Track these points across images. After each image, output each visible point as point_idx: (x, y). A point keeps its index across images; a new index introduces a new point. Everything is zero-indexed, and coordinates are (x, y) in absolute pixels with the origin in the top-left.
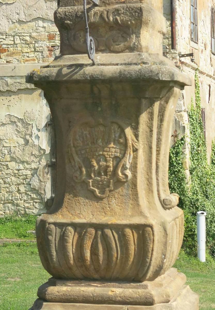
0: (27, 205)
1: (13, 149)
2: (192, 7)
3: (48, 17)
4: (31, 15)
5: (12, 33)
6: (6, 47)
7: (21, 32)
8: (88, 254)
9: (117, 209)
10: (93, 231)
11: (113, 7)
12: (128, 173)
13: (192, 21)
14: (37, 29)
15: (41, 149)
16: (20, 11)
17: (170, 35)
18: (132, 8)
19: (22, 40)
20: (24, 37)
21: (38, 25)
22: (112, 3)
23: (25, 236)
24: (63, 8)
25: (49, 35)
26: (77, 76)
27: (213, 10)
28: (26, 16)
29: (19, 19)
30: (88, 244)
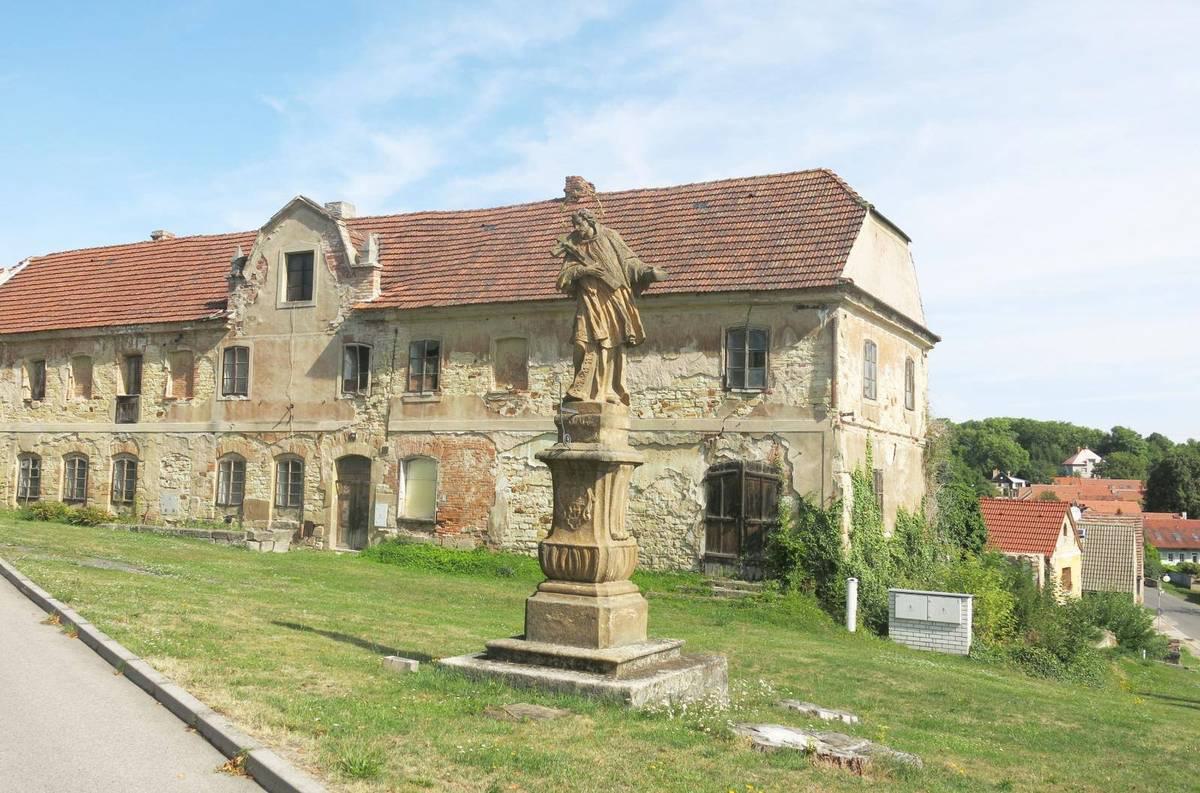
0: (681, 560)
1: (670, 504)
8: (554, 561)
9: (582, 538)
10: (566, 549)
12: (589, 515)
15: (697, 504)
23: (673, 591)
26: (559, 457)
30: (564, 557)
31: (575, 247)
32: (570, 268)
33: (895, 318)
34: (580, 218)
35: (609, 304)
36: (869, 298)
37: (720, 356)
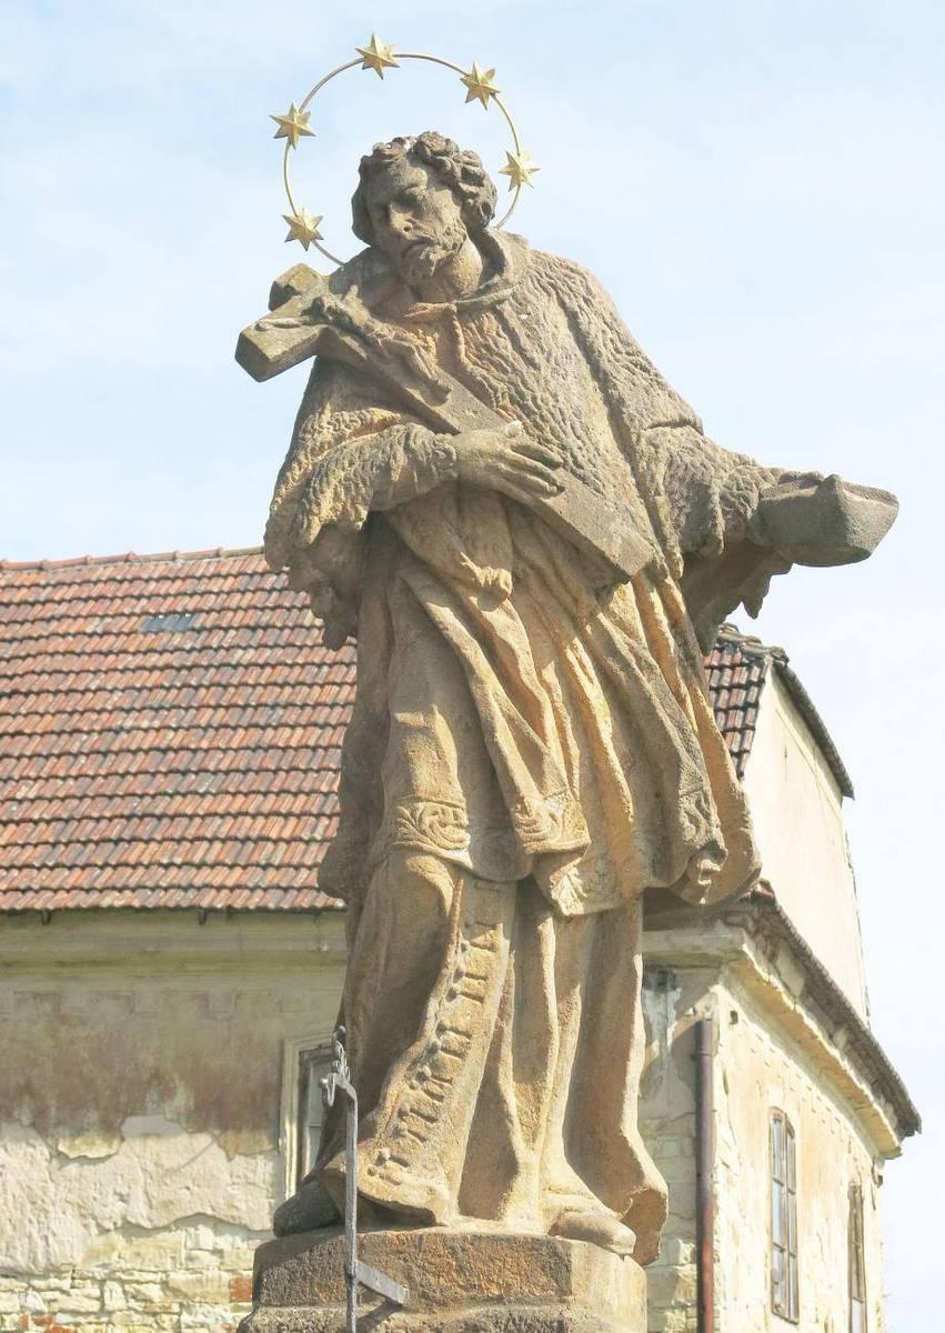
2: (776, 1186)
3: (235, 1213)
4: (172, 1203)
5: (96, 1269)
6: (67, 1324)
7: (129, 1266)
11: (461, 1318)
13: (777, 1239)
14: (190, 1259)
16: (129, 1188)
17: (694, 1296)
18: (529, 1322)
19: (133, 1297)
20: (142, 1288)
21: (197, 1243)
22: (455, 1300)
24: (272, 1311)
25: (237, 1281)
27: (855, 1192)
28: (151, 1207)
29: (124, 1218)
31: (384, 330)
32: (361, 439)
33: (841, 1037)
34: (421, 175)
35: (578, 655)
36: (800, 956)
37: (278, 1151)
